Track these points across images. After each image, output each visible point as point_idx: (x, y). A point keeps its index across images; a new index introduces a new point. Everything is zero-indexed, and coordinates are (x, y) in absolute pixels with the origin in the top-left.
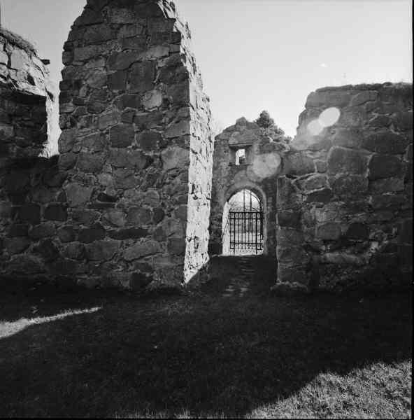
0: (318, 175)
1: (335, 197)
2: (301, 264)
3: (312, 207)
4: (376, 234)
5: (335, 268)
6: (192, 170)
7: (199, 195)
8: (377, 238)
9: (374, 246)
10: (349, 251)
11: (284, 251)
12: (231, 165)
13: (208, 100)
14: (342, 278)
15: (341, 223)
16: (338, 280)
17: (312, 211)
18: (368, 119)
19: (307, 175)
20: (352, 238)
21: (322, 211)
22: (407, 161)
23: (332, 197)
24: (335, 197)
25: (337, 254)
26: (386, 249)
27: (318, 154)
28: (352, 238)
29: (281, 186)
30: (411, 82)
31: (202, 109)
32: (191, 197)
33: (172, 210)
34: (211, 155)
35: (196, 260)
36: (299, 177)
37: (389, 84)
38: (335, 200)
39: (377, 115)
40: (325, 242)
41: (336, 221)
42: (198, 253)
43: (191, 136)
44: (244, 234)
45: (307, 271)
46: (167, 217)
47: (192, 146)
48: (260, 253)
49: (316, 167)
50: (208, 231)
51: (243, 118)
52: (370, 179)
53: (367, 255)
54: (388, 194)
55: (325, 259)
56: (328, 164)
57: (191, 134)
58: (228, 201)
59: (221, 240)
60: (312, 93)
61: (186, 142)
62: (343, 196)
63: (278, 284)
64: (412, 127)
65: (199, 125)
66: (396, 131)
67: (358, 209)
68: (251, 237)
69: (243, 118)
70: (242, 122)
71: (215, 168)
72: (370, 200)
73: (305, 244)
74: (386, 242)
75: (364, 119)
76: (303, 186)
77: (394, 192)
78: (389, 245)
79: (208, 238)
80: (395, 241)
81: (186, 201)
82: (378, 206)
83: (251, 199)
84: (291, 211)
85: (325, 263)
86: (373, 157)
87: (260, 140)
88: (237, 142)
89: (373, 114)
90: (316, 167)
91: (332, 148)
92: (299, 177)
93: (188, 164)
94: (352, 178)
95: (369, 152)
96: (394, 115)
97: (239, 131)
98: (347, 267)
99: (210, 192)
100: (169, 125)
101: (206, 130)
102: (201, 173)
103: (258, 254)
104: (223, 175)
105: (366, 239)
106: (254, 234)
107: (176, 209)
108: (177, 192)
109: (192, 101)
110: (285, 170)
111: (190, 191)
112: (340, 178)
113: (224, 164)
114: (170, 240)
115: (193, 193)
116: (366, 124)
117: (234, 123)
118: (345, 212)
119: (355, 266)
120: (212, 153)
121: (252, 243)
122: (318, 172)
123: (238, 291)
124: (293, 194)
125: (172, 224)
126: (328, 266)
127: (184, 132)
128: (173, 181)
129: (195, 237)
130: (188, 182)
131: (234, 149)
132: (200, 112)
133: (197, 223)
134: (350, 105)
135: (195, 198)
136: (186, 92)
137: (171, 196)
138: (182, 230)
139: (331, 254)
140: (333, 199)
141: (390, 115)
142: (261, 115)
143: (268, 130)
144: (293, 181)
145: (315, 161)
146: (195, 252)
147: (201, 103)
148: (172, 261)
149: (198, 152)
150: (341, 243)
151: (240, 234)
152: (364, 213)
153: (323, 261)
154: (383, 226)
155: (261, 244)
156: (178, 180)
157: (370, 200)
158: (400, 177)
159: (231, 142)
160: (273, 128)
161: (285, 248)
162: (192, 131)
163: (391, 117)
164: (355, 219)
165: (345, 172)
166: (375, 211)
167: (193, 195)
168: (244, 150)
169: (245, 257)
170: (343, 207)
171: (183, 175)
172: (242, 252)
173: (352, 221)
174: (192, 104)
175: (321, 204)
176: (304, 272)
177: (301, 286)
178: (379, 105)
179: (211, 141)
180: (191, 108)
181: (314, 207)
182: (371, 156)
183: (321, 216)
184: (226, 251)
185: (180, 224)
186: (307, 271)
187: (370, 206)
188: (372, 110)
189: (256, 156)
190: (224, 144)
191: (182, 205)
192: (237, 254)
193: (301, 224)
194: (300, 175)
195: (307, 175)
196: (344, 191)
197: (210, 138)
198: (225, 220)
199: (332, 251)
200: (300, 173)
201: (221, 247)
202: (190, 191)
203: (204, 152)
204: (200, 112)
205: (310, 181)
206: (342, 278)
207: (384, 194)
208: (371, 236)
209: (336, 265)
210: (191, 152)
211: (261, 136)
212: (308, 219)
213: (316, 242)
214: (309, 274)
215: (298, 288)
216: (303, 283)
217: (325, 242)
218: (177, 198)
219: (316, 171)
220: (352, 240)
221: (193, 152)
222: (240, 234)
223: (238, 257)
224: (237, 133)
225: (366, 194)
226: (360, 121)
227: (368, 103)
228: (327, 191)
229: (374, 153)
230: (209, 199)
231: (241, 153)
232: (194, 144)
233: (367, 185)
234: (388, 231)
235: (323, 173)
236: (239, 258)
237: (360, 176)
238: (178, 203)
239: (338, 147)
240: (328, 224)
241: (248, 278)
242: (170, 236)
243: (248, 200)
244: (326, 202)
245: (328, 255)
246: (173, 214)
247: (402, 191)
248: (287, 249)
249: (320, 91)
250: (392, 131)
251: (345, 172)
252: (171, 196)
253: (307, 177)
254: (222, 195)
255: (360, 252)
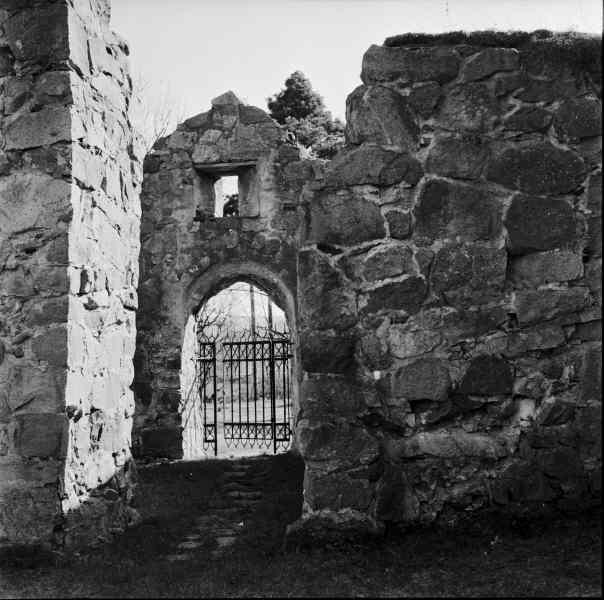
0: (393, 244)
1: (434, 296)
2: (357, 464)
3: (380, 322)
4: (527, 383)
5: (441, 469)
6: (77, 232)
7: (100, 298)
8: (530, 391)
9: (526, 409)
10: (470, 427)
11: (316, 432)
12: (200, 217)
13: (125, 50)
14: (456, 491)
15: (450, 359)
16: (445, 497)
17: (380, 332)
18: (499, 111)
19: (366, 244)
20: (475, 396)
21: (404, 331)
22: (587, 212)
23: (426, 297)
24: (434, 296)
25: (442, 434)
26: (552, 418)
27: (391, 194)
28: (476, 395)
29: (306, 273)
30: (599, 32)
31: (107, 74)
32: (76, 304)
33: (26, 338)
34: (135, 195)
35: (94, 463)
36: (348, 250)
37: (544, 34)
38: (432, 305)
39: (518, 105)
40: (416, 405)
41: (438, 356)
42: (101, 451)
43: (76, 147)
44: (252, 404)
45: (373, 480)
46: (11, 358)
47: (77, 172)
48: (283, 448)
49: (386, 225)
50: (130, 395)
51: (230, 96)
52: (514, 255)
53: (511, 433)
54: (550, 286)
55: (416, 447)
56: (414, 219)
57: (75, 137)
58: (195, 312)
59: (179, 418)
60: (374, 47)
61: (61, 161)
62: (450, 294)
63: (305, 517)
64: (601, 132)
65: (98, 117)
66: (561, 142)
67: (485, 323)
68: (261, 411)
69: (230, 96)
70: (225, 106)
71: (150, 228)
72: (512, 302)
73: (367, 412)
74: (551, 400)
75: (492, 114)
76: (359, 272)
77: (562, 283)
78: (556, 408)
79: (131, 411)
80: (568, 398)
81: (62, 314)
82: (532, 314)
83: (270, 310)
84: (332, 333)
85: (413, 459)
86: (515, 201)
87: (274, 153)
88: (215, 158)
89: (511, 101)
90: (386, 225)
91: (422, 181)
92: (348, 250)
93: (67, 218)
94: (471, 251)
95: (504, 190)
96: (556, 105)
97: (220, 128)
98: (467, 464)
99: (133, 290)
100: (15, 116)
101: (118, 129)
102: (105, 242)
103: (280, 451)
104: (180, 246)
105: (508, 395)
106: (268, 404)
107: (36, 335)
108: (37, 292)
109: (77, 54)
110: (314, 233)
111: (75, 286)
112: (443, 252)
113: (183, 217)
114: (20, 419)
115: (81, 293)
116: (497, 124)
117: (208, 108)
118: (457, 332)
119: (486, 461)
120: (139, 189)
121: (264, 425)
122: (393, 236)
123: (210, 544)
124: (335, 291)
125: (25, 376)
126: (422, 465)
127: (54, 135)
128: (28, 264)
129: (93, 410)
130: (66, 263)
131: (209, 176)
132: (100, 82)
133: (99, 368)
134: (461, 79)
135: (90, 306)
136: (57, 31)
137: (24, 301)
138: (54, 390)
139: (430, 436)
140: (429, 301)
141: (548, 104)
142: (289, 83)
143: (308, 126)
144: (333, 260)
145: (384, 211)
146: (94, 448)
147: (101, 59)
148: (27, 477)
149: (97, 186)
150: (454, 407)
151: (244, 405)
152: (499, 334)
153: (410, 453)
154: (546, 362)
155: (285, 425)
156: (40, 259)
157: (512, 302)
158: (573, 248)
159: (203, 155)
160: (320, 120)
161: (319, 425)
162: (76, 132)
163: (548, 109)
164: (480, 347)
165: (453, 237)
166: (525, 327)
167: (84, 299)
168: (235, 178)
169: (243, 461)
170: (451, 320)
171: (53, 247)
172: (237, 449)
173: (473, 354)
174: (76, 62)
175: (403, 312)
176: (366, 482)
177: (359, 516)
178: (524, 81)
179: (133, 158)
180: (73, 75)
181: (387, 320)
182: (511, 198)
183: (402, 341)
184: (194, 448)
185: (47, 375)
186: (373, 480)
187: (513, 316)
188: (508, 93)
189: (263, 193)
190: (172, 169)
191: (53, 326)
192: (220, 456)
193: (357, 365)
194: (350, 245)
195: (366, 244)
196: (459, 282)
197: (130, 149)
198: (189, 372)
199: (431, 427)
200: (349, 241)
201: (176, 437)
202: (75, 286)
203: (114, 187)
204: (100, 82)
205: (374, 259)
206: (456, 491)
207: (542, 288)
208: (517, 388)
209: (441, 460)
210: (75, 189)
211: (280, 143)
212: (372, 351)
213: (393, 406)
214: (378, 486)
215: (352, 521)
216: (365, 510)
217: (416, 405)
218: (39, 307)
219: (388, 233)
220: (474, 399)
221: (83, 187)
222: (244, 405)
223: (225, 461)
224: (213, 134)
225: (503, 290)
226: (484, 118)
227: (497, 76)
228: (415, 282)
229: (517, 192)
230: (131, 309)
231: (228, 186)
232: (81, 165)
233: (504, 266)
234: (554, 373)
235: (404, 238)
236: (226, 465)
237: (488, 245)
238: (41, 320)
239: (435, 177)
240: (419, 362)
241: (244, 513)
242: (20, 408)
243: (261, 313)
244: (413, 307)
245: (424, 439)
246: (28, 350)
247: (578, 280)
248: (323, 428)
249: (393, 43)
250: (554, 141)
251: (453, 237)
252: (24, 301)
253: (367, 250)
254: (179, 300)
255: (497, 428)
